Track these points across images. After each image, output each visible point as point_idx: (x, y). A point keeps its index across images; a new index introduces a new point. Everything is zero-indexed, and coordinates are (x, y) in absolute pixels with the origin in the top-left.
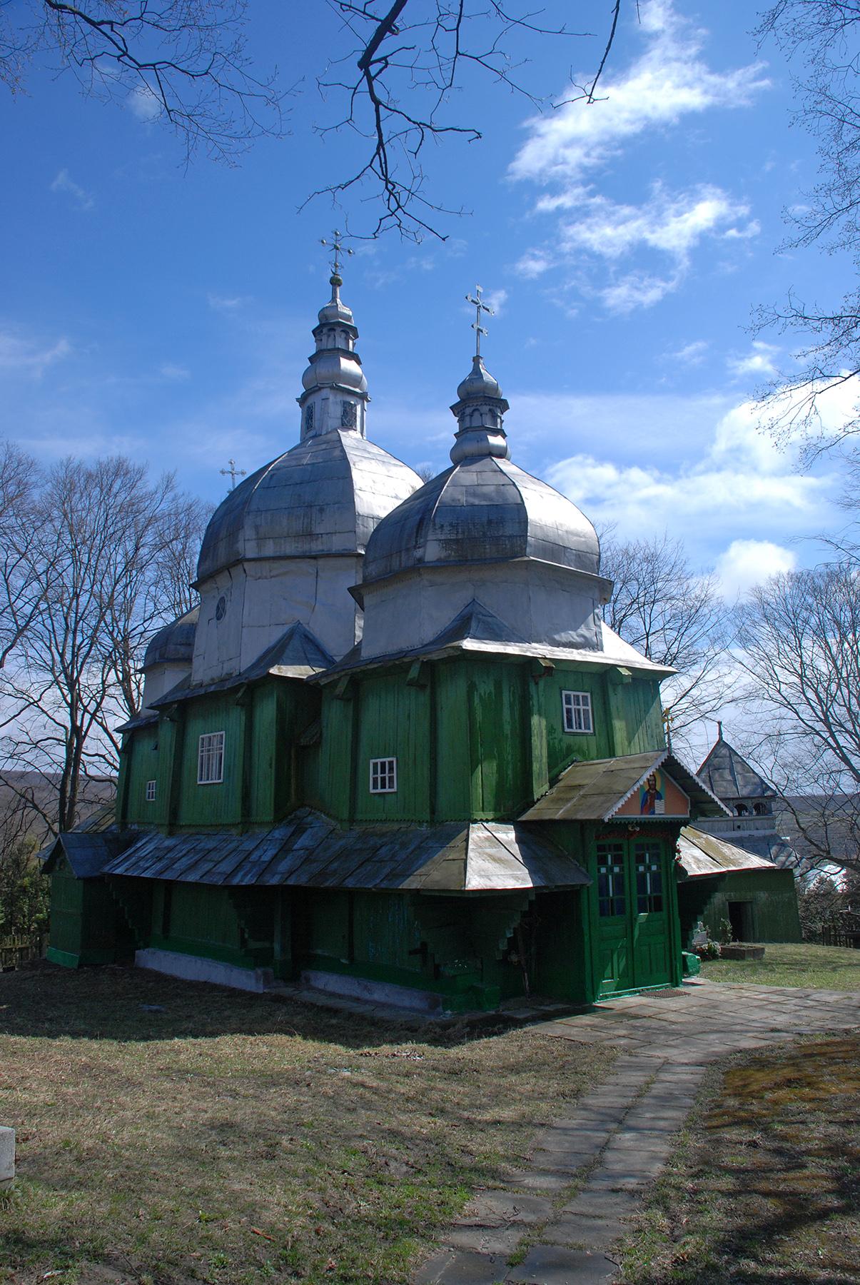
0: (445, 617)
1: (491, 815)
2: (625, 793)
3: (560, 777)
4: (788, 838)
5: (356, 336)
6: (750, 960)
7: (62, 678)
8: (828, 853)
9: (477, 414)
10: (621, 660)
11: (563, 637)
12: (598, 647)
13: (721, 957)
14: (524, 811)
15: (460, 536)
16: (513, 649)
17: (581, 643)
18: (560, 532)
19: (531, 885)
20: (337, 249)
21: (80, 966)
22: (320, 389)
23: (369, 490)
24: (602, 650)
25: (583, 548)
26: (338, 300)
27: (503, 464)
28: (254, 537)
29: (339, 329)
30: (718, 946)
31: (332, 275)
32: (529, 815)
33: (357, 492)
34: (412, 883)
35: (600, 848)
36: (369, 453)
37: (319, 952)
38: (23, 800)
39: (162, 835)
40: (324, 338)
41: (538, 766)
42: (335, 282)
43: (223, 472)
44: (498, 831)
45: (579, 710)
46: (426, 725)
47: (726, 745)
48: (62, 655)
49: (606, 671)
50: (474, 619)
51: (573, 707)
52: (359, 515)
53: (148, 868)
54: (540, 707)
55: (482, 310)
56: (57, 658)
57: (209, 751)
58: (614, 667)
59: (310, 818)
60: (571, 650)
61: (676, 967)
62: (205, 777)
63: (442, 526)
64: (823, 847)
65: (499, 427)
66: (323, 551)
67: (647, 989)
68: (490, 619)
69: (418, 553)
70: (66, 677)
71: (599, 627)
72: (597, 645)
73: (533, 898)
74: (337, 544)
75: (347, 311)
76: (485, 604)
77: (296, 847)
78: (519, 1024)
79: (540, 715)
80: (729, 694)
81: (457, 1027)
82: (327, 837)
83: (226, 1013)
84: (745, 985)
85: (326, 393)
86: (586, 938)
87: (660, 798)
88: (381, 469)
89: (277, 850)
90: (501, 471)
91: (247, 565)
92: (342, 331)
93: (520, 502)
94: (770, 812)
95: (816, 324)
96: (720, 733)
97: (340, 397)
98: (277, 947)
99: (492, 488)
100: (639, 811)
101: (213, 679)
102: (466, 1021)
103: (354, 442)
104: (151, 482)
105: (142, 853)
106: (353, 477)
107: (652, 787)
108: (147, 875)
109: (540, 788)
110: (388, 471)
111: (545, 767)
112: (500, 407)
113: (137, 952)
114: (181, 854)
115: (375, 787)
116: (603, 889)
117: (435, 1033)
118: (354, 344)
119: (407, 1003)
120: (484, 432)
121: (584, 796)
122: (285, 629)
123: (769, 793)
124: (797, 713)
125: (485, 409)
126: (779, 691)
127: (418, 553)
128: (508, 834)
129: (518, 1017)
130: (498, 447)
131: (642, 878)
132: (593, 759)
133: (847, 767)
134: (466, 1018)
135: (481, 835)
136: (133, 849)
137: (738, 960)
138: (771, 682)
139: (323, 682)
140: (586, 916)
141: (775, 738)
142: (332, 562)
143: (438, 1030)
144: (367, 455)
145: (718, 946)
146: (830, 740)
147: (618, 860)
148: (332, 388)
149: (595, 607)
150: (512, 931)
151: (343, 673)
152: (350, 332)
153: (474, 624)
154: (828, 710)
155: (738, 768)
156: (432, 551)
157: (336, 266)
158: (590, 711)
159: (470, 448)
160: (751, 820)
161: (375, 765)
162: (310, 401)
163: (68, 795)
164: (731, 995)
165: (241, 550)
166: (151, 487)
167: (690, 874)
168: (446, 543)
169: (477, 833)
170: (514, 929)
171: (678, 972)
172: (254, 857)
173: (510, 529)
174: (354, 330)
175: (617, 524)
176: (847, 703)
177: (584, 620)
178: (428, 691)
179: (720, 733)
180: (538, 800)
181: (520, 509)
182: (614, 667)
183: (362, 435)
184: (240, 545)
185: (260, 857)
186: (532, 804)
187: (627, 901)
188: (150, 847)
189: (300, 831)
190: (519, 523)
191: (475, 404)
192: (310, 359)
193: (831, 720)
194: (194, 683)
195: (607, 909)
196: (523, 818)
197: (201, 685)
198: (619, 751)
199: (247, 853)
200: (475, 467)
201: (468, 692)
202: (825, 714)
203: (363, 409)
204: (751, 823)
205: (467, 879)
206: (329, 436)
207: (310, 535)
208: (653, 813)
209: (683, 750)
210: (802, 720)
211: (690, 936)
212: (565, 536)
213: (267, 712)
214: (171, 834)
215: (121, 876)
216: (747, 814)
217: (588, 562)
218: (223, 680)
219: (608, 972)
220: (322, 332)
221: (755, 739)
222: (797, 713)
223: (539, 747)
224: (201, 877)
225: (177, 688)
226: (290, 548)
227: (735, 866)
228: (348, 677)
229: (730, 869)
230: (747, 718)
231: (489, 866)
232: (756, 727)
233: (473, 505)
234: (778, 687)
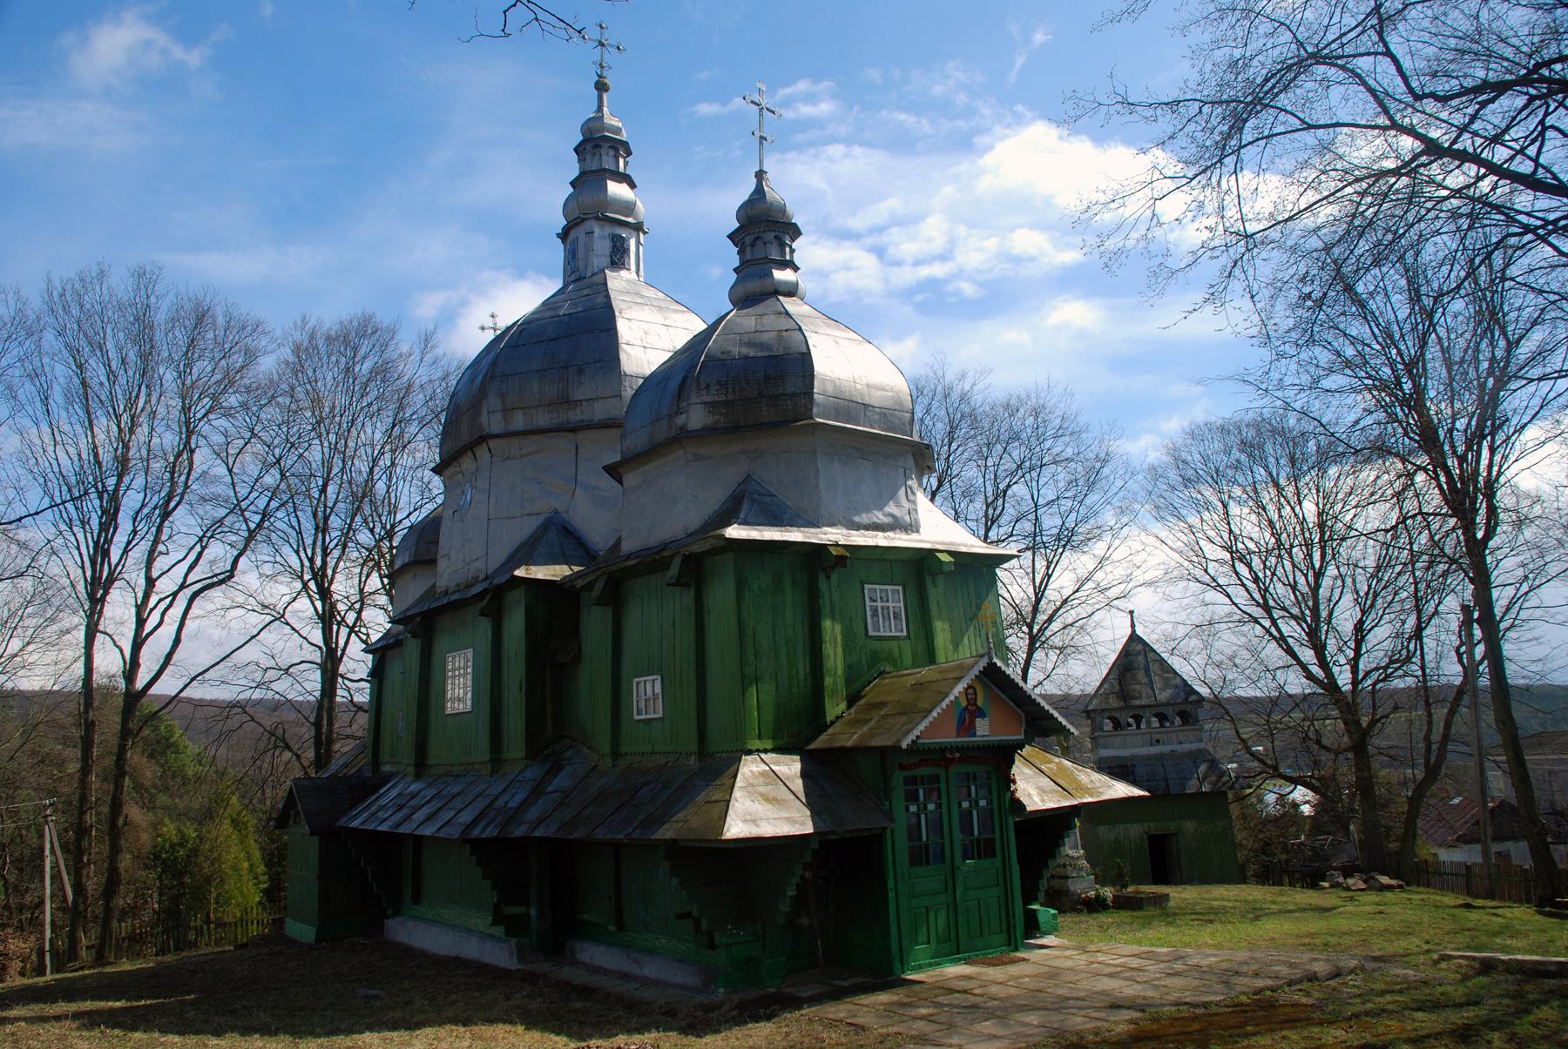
0: (715, 497)
1: (769, 745)
2: (931, 711)
3: (863, 693)
4: (1261, 748)
5: (629, 153)
6: (1152, 911)
7: (312, 585)
8: (1275, 768)
9: (759, 243)
10: (937, 543)
11: (864, 518)
12: (913, 527)
13: (1113, 907)
14: (815, 736)
15: (730, 397)
16: (795, 535)
17: (889, 524)
18: (858, 386)
19: (809, 829)
20: (602, 45)
21: (318, 940)
22: (583, 220)
23: (640, 343)
24: (918, 531)
26: (605, 109)
27: (790, 304)
28: (500, 408)
30: (1108, 892)
31: (596, 78)
32: (821, 742)
33: (623, 347)
34: (666, 832)
35: (910, 781)
36: (642, 297)
37: (586, 917)
38: (273, 739)
39: (410, 779)
40: (588, 157)
41: (831, 680)
42: (601, 87)
43: (483, 328)
44: (776, 763)
45: (888, 608)
46: (690, 634)
47: (1140, 639)
48: (311, 560)
49: (922, 558)
50: (746, 500)
52: (626, 375)
53: (385, 820)
54: (832, 607)
55: (765, 111)
56: (307, 563)
58: (931, 553)
59: (569, 753)
60: (875, 533)
61: (1015, 926)
63: (708, 385)
64: (1269, 762)
65: (788, 258)
66: (583, 421)
67: (976, 956)
68: (768, 499)
69: (680, 420)
70: (317, 584)
71: (914, 502)
72: (911, 525)
73: (815, 845)
74: (600, 411)
75: (615, 122)
76: (763, 481)
77: (549, 789)
78: (795, 1003)
79: (833, 618)
80: (1140, 577)
81: (724, 1008)
82: (587, 776)
83: (453, 997)
84: (1102, 946)
86: (891, 894)
87: (983, 715)
88: (657, 317)
90: (787, 313)
91: (492, 443)
92: (610, 147)
93: (805, 350)
94: (1198, 721)
95: (1149, 112)
96: (1133, 626)
97: (609, 230)
98: (533, 912)
99: (773, 335)
100: (954, 732)
101: (458, 585)
102: (736, 1002)
103: (624, 284)
104: (405, 343)
105: (383, 802)
106: (618, 328)
107: (972, 702)
108: (383, 828)
109: (835, 708)
110: (665, 319)
111: (841, 682)
112: (788, 233)
113: (386, 921)
114: (423, 801)
117: (696, 1017)
118: (626, 164)
119: (679, 979)
120: (768, 266)
121: (885, 717)
122: (541, 519)
123: (1193, 698)
124: (1228, 596)
126: (1206, 571)
127: (680, 420)
128: (790, 767)
129: (802, 994)
130: (786, 283)
131: (966, 817)
132: (907, 669)
133: (1295, 662)
134: (736, 999)
135: (755, 769)
136: (376, 796)
137: (1134, 910)
138: (1195, 559)
139: (580, 583)
140: (890, 866)
141: (1207, 628)
142: (593, 435)
143: (699, 1013)
144: (639, 300)
145: (1108, 892)
146: (1273, 630)
148: (597, 219)
149: (907, 478)
150: (795, 887)
151: (599, 572)
152: (621, 148)
153: (746, 506)
154: (1266, 590)
155: (1154, 668)
156: (696, 417)
157: (602, 67)
159: (754, 286)
160: (1173, 732)
161: (638, 683)
163: (324, 730)
164: (1081, 960)
165: (485, 425)
166: (405, 348)
167: (1028, 809)
168: (712, 406)
169: (750, 767)
170: (797, 885)
171: (1018, 933)
172: (499, 803)
173: (791, 386)
174: (625, 145)
175: (991, 370)
176: (1291, 580)
177: (893, 495)
178: (692, 592)
179: (1133, 626)
180: (832, 723)
181: (805, 359)
182: (932, 552)
183: (638, 275)
184: (484, 418)
185: (507, 802)
186: (824, 727)
187: (998, 841)
188: (394, 793)
189: (555, 769)
190: (803, 377)
191: (757, 231)
192: (573, 184)
193: (1271, 603)
194: (439, 590)
195: (919, 856)
196: (812, 746)
197: (446, 593)
198: (941, 657)
199: (492, 798)
200: (759, 309)
201: (737, 590)
202: (1264, 597)
203: (638, 243)
205: (726, 825)
206: (594, 279)
207: (566, 402)
208: (974, 735)
209: (1089, 648)
210: (1236, 605)
212: (865, 390)
213: (515, 624)
214: (418, 776)
215: (355, 830)
216: (1168, 724)
217: (896, 421)
218: (469, 586)
219: (922, 936)
220: (585, 149)
221: (1182, 631)
222: (1228, 596)
223: (832, 657)
224: (439, 829)
225: (423, 598)
226: (543, 419)
227: (1091, 796)
228: (606, 577)
229: (1085, 800)
230: (1168, 606)
231: (760, 808)
232: (1182, 616)
233: (746, 357)
234: (1204, 565)
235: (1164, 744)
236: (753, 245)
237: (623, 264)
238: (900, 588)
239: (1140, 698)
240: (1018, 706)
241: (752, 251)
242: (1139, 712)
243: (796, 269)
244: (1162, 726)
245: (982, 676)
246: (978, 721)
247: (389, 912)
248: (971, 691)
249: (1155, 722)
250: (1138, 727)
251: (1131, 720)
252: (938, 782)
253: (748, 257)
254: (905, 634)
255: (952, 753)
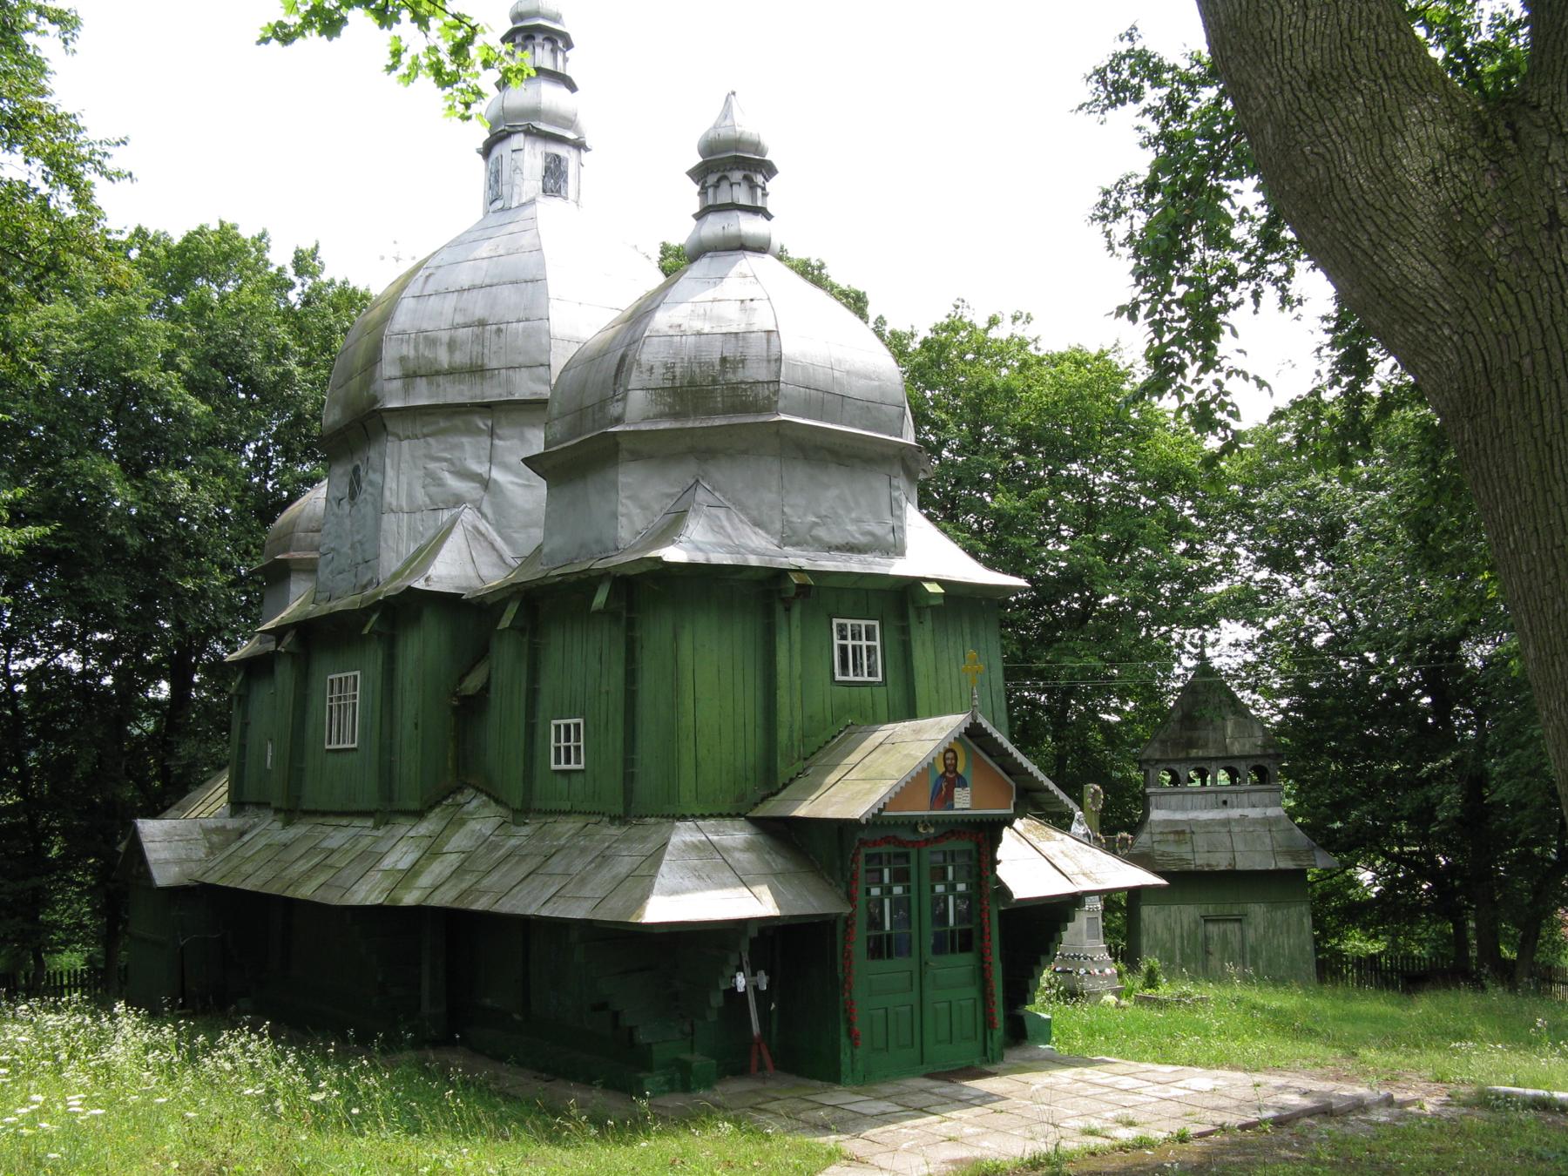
17: (866, 545)
18: (837, 374)
25: (876, 396)
29: (539, 39)
35: (870, 858)
37: (488, 1002)
51: (850, 643)
57: (339, 698)
62: (334, 738)
71: (900, 518)
85: (518, 140)
87: (964, 785)
89: (421, 853)
100: (927, 802)
112: (761, 172)
115: (558, 762)
116: (875, 922)
125: (737, 176)
147: (900, 876)
158: (879, 648)
161: (558, 727)
162: (496, 152)
167: (1017, 896)
184: (74, 654)
195: (880, 948)
204: (1245, 796)
208: (952, 807)
211: (1031, 987)
235: (1232, 807)
236: (716, 186)
237: (559, 191)
238: (876, 623)
239: (1205, 746)
240: (1009, 774)
241: (715, 194)
242: (1202, 765)
243: (768, 216)
244: (1233, 782)
245: (966, 738)
246: (958, 792)
247: (71, 960)
248: (950, 755)
249: (1223, 777)
250: (1204, 783)
251: (1192, 774)
252: (908, 861)
253: (710, 202)
254: (880, 679)
255: (925, 827)
